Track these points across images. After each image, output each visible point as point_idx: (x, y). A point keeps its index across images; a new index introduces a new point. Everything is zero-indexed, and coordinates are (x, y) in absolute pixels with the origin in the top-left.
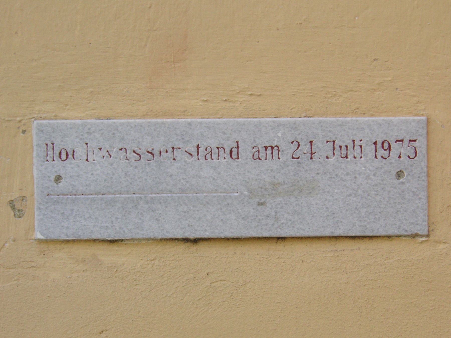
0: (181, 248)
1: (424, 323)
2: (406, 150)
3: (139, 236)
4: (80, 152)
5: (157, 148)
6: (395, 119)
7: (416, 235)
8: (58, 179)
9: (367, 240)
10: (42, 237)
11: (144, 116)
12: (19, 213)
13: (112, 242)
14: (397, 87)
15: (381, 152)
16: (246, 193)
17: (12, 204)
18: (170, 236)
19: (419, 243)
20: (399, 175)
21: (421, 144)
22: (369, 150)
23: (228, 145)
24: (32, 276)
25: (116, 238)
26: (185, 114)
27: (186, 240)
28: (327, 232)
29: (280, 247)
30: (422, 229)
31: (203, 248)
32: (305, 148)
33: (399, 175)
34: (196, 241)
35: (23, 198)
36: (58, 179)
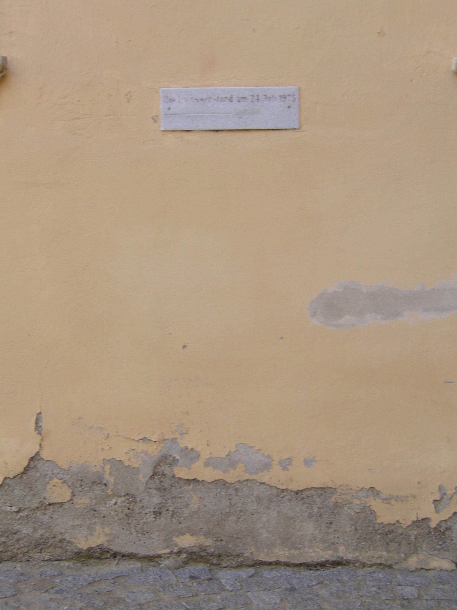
0: (213, 133)
1: (26, 550)
2: (291, 98)
3: (197, 129)
4: (177, 100)
5: (204, 97)
6: (287, 87)
7: (295, 129)
8: (169, 109)
9: (277, 131)
10: (163, 129)
11: (200, 86)
12: (155, 121)
13: (188, 131)
14: (107, 484)
15: (283, 99)
16: (235, 114)
17: (153, 118)
18: (208, 129)
19: (296, 132)
20: (289, 107)
21: (297, 96)
22: (278, 98)
23: (229, 96)
24: (172, 431)
25: (190, 130)
26: (213, 86)
27: (214, 131)
28: (263, 128)
29: (247, 134)
30: (297, 127)
31: (220, 133)
32: (256, 98)
33: (289, 107)
34: (217, 131)
35: (157, 116)
36: (169, 109)
